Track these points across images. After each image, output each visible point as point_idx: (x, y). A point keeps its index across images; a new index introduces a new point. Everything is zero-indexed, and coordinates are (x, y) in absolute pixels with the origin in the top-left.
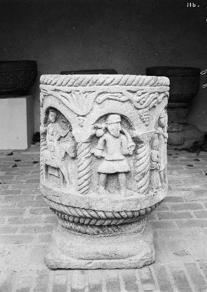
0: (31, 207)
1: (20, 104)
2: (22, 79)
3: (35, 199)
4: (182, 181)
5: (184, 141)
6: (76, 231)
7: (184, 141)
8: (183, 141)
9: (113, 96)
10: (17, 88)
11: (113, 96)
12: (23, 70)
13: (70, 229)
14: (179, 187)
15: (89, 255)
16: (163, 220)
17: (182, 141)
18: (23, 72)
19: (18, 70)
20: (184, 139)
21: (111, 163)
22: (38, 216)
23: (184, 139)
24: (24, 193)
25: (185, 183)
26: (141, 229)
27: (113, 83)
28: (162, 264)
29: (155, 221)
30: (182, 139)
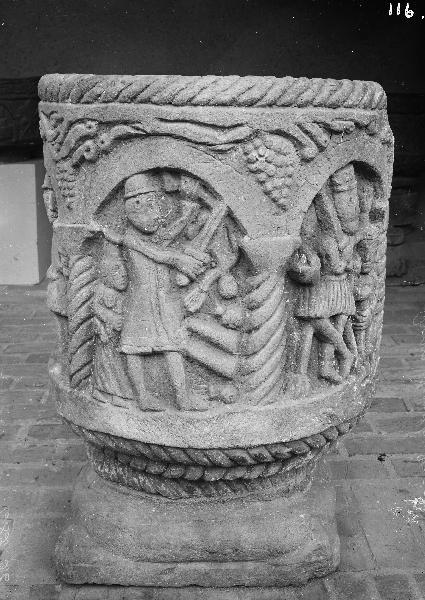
0: (31, 422)
1: (28, 169)
2: (24, 119)
3: (43, 401)
4: (403, 361)
5: (407, 267)
6: (133, 486)
7: (407, 267)
8: (404, 267)
9: (7, 99)
10: (14, 140)
11: (7, 99)
12: (26, 99)
13: (118, 480)
14: (395, 376)
15: (164, 552)
16: (358, 457)
17: (401, 267)
18: (28, 101)
19: (14, 96)
20: (407, 262)
21: (221, 109)
22: (48, 442)
23: (407, 262)
24: (19, 385)
25: (411, 365)
26: (305, 483)
27: (259, 103)
28: (358, 576)
29: (338, 458)
30: (403, 262)
